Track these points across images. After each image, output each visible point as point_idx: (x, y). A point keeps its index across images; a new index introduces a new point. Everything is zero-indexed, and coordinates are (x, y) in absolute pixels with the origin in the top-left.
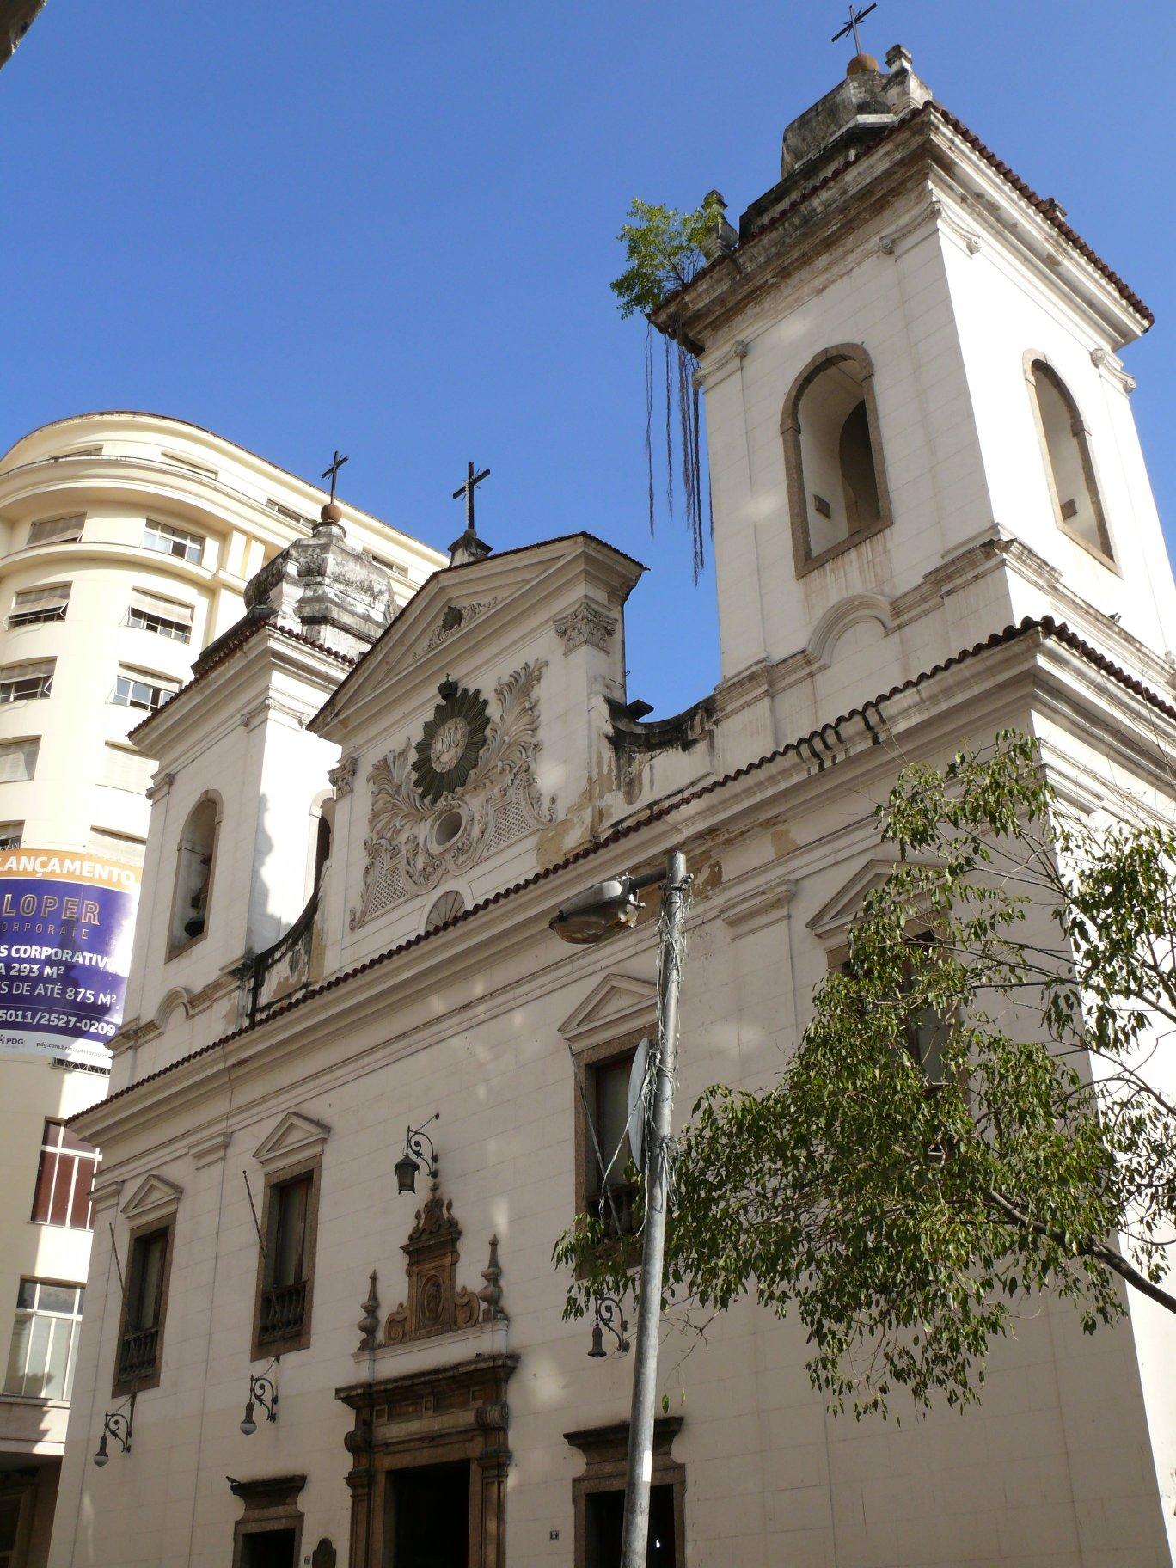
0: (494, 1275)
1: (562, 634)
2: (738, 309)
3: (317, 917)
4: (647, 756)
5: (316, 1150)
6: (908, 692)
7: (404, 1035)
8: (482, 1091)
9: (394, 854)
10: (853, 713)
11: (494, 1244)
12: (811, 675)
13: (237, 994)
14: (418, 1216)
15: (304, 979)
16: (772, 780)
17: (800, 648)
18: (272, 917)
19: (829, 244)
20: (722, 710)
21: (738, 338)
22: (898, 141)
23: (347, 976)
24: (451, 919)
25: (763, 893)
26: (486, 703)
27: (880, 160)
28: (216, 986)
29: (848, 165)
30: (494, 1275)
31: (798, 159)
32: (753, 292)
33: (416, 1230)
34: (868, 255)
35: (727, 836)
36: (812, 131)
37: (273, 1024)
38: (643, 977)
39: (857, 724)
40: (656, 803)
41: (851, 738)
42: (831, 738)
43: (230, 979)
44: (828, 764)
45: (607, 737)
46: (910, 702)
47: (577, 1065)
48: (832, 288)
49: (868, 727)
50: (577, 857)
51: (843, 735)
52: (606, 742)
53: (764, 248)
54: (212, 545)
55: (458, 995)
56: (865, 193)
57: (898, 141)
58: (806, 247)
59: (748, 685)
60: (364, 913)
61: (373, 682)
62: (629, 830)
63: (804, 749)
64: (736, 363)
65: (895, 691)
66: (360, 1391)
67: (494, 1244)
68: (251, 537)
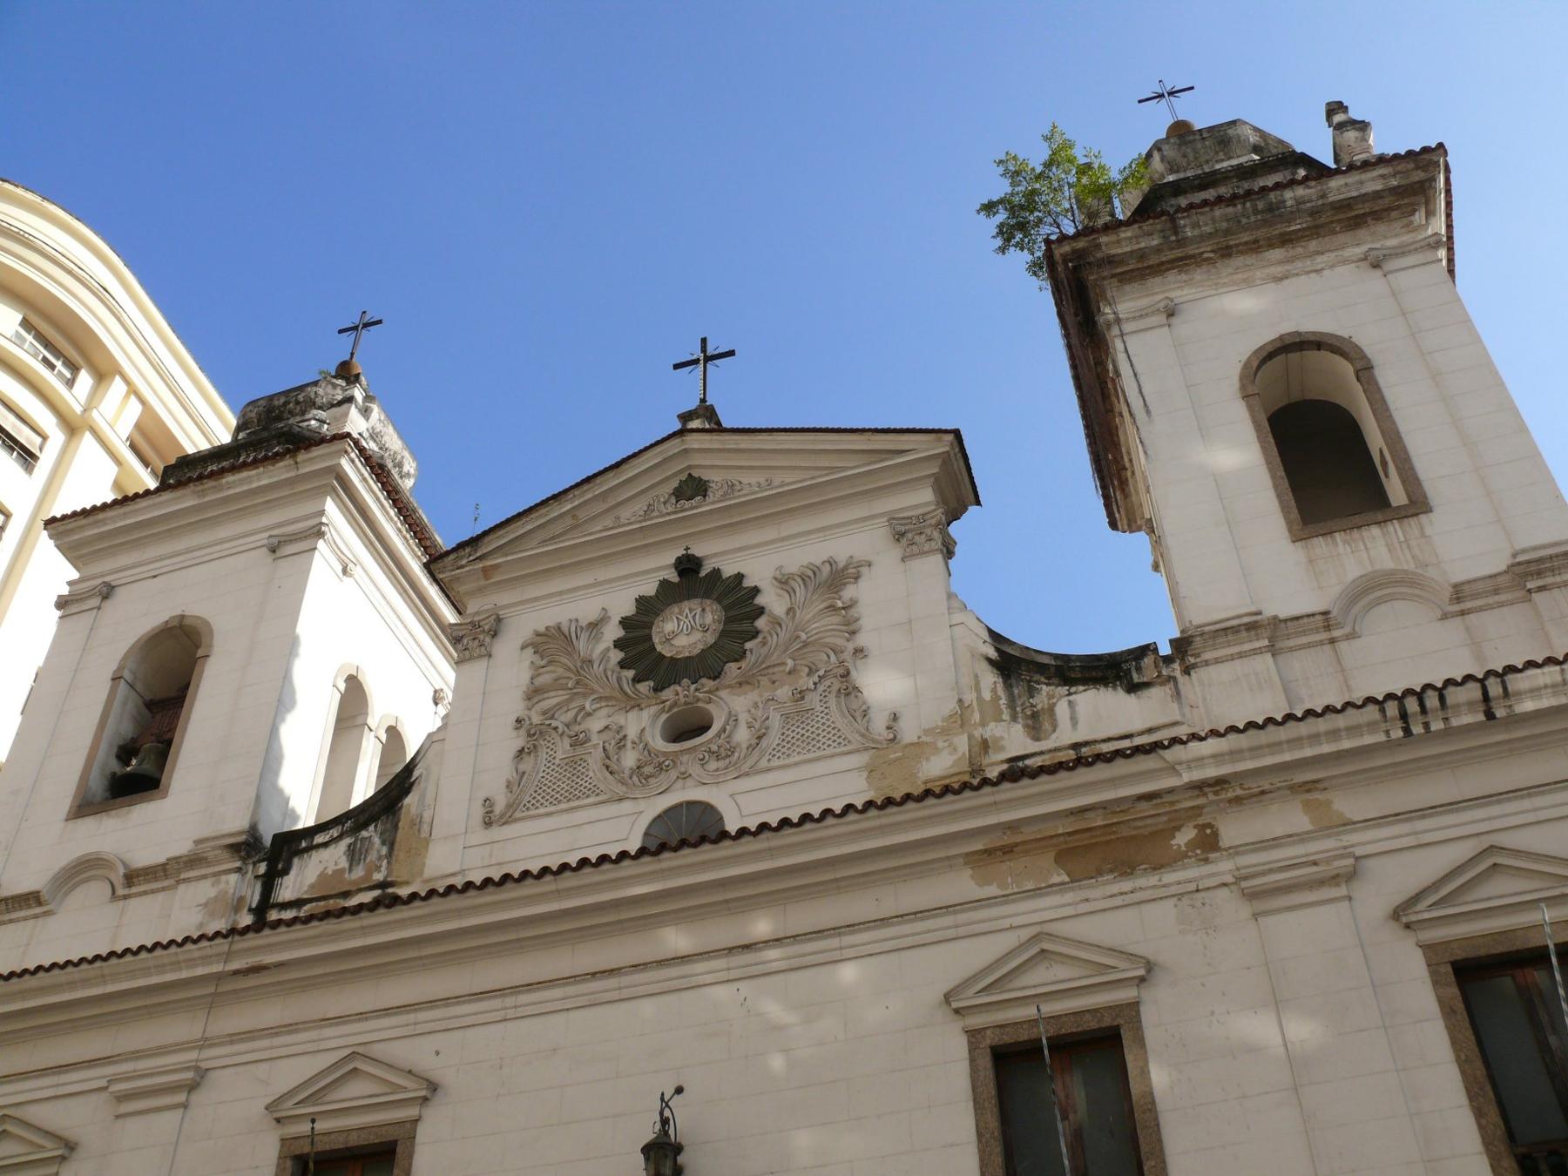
1: (899, 536)
2: (1159, 269)
3: (410, 801)
4: (1064, 690)
5: (412, 1112)
6: (1546, 669)
7: (611, 972)
8: (777, 1063)
9: (578, 741)
10: (1469, 678)
12: (1332, 641)
13: (234, 877)
15: (379, 877)
16: (1334, 734)
17: (1322, 608)
18: (280, 792)
19: (1286, 240)
20: (1198, 655)
21: (1172, 295)
22: (1399, 168)
23: (469, 885)
24: (691, 830)
25: (1315, 863)
26: (756, 591)
27: (1373, 179)
28: (193, 861)
29: (1293, 183)
31: (1172, 171)
32: (1181, 259)
34: (1345, 262)
35: (1239, 792)
36: (1195, 151)
37: (299, 932)
38: (47, 1128)
39: (1473, 691)
40: (1086, 744)
41: (1457, 706)
42: (1432, 700)
43: (226, 855)
44: (1417, 729)
45: (989, 660)
46: (1548, 681)
47: (973, 1048)
48: (1294, 280)
49: (1486, 698)
50: (947, 790)
51: (1449, 701)
52: (985, 665)
53: (1213, 219)
54: (85, 379)
55: (723, 932)
56: (1346, 205)
57: (1399, 168)
58: (1260, 234)
59: (1244, 634)
60: (511, 806)
61: (540, 536)
62: (1100, 758)
63: (1392, 709)
64: (1162, 318)
65: (1531, 664)
68: (133, 391)
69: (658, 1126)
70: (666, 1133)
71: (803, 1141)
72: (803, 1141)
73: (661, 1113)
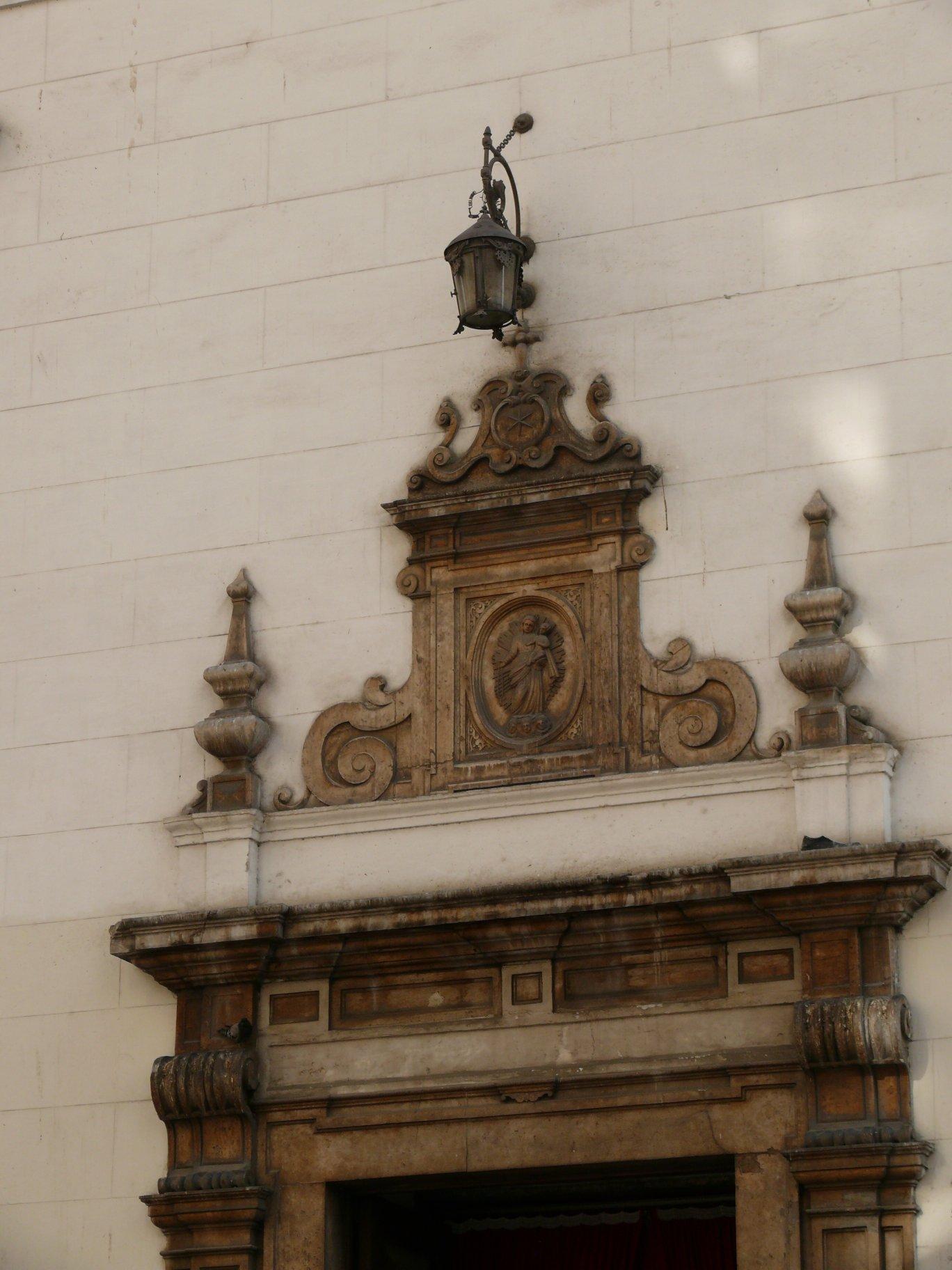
0: (823, 610)
11: (819, 519)
14: (448, 418)
30: (823, 610)
33: (442, 458)
66: (239, 932)
67: (819, 519)
69: (479, 202)
70: (498, 216)
71: (796, 226)
72: (796, 226)
73: (486, 175)
